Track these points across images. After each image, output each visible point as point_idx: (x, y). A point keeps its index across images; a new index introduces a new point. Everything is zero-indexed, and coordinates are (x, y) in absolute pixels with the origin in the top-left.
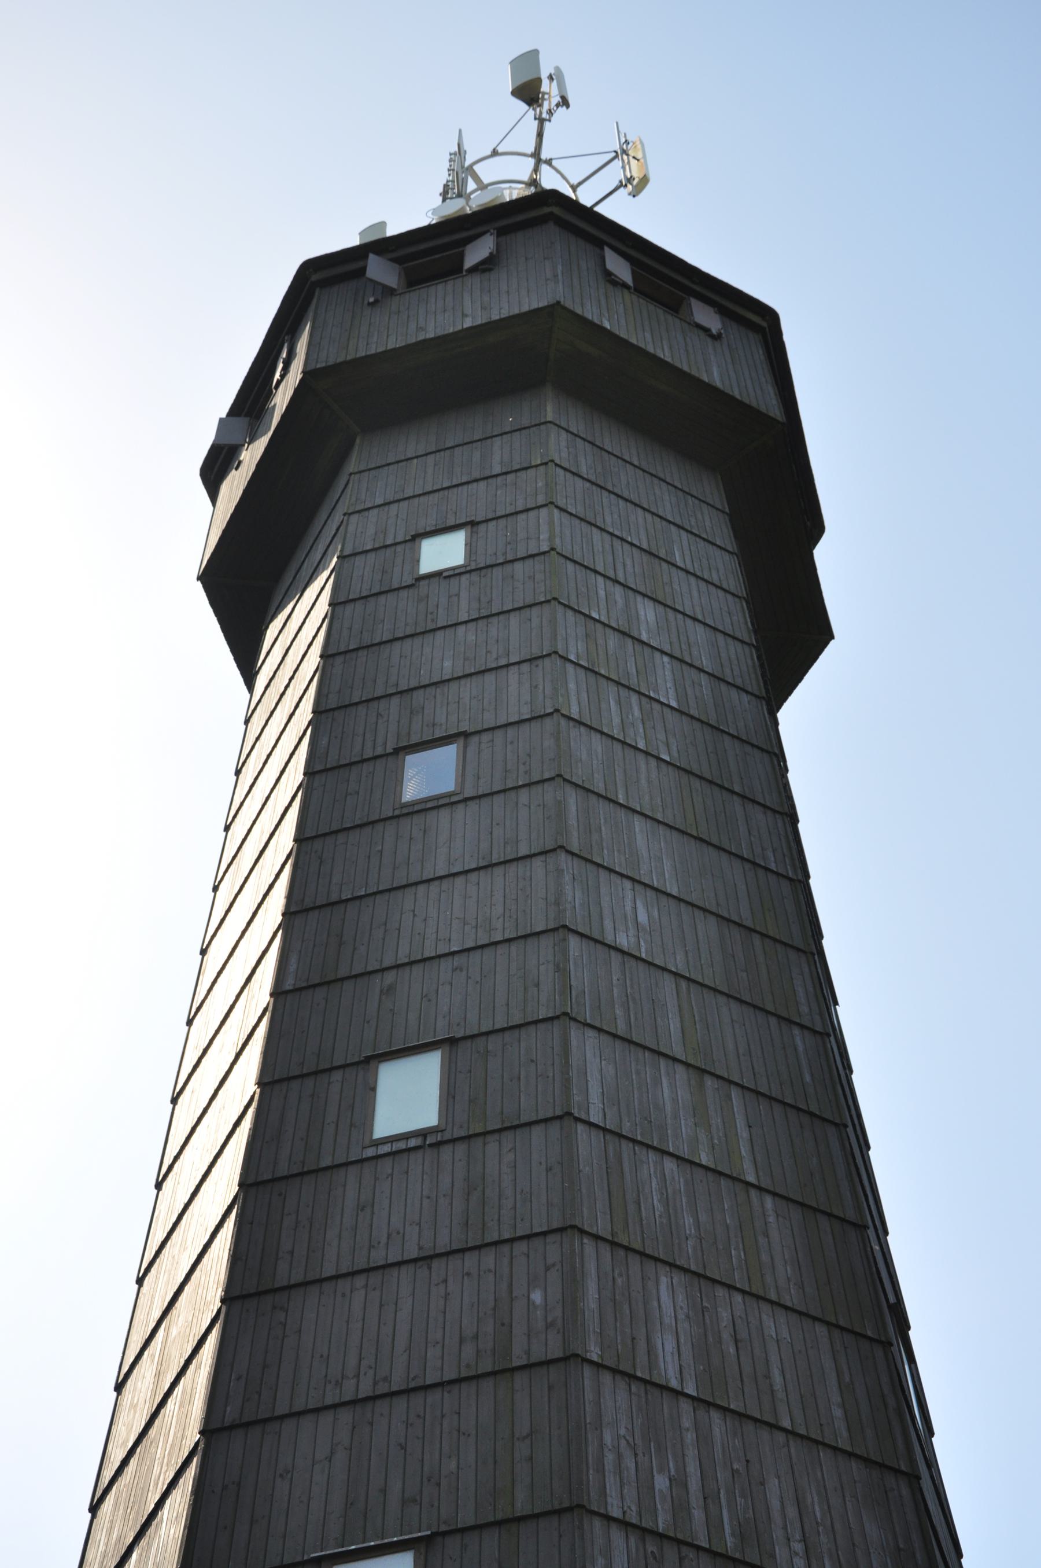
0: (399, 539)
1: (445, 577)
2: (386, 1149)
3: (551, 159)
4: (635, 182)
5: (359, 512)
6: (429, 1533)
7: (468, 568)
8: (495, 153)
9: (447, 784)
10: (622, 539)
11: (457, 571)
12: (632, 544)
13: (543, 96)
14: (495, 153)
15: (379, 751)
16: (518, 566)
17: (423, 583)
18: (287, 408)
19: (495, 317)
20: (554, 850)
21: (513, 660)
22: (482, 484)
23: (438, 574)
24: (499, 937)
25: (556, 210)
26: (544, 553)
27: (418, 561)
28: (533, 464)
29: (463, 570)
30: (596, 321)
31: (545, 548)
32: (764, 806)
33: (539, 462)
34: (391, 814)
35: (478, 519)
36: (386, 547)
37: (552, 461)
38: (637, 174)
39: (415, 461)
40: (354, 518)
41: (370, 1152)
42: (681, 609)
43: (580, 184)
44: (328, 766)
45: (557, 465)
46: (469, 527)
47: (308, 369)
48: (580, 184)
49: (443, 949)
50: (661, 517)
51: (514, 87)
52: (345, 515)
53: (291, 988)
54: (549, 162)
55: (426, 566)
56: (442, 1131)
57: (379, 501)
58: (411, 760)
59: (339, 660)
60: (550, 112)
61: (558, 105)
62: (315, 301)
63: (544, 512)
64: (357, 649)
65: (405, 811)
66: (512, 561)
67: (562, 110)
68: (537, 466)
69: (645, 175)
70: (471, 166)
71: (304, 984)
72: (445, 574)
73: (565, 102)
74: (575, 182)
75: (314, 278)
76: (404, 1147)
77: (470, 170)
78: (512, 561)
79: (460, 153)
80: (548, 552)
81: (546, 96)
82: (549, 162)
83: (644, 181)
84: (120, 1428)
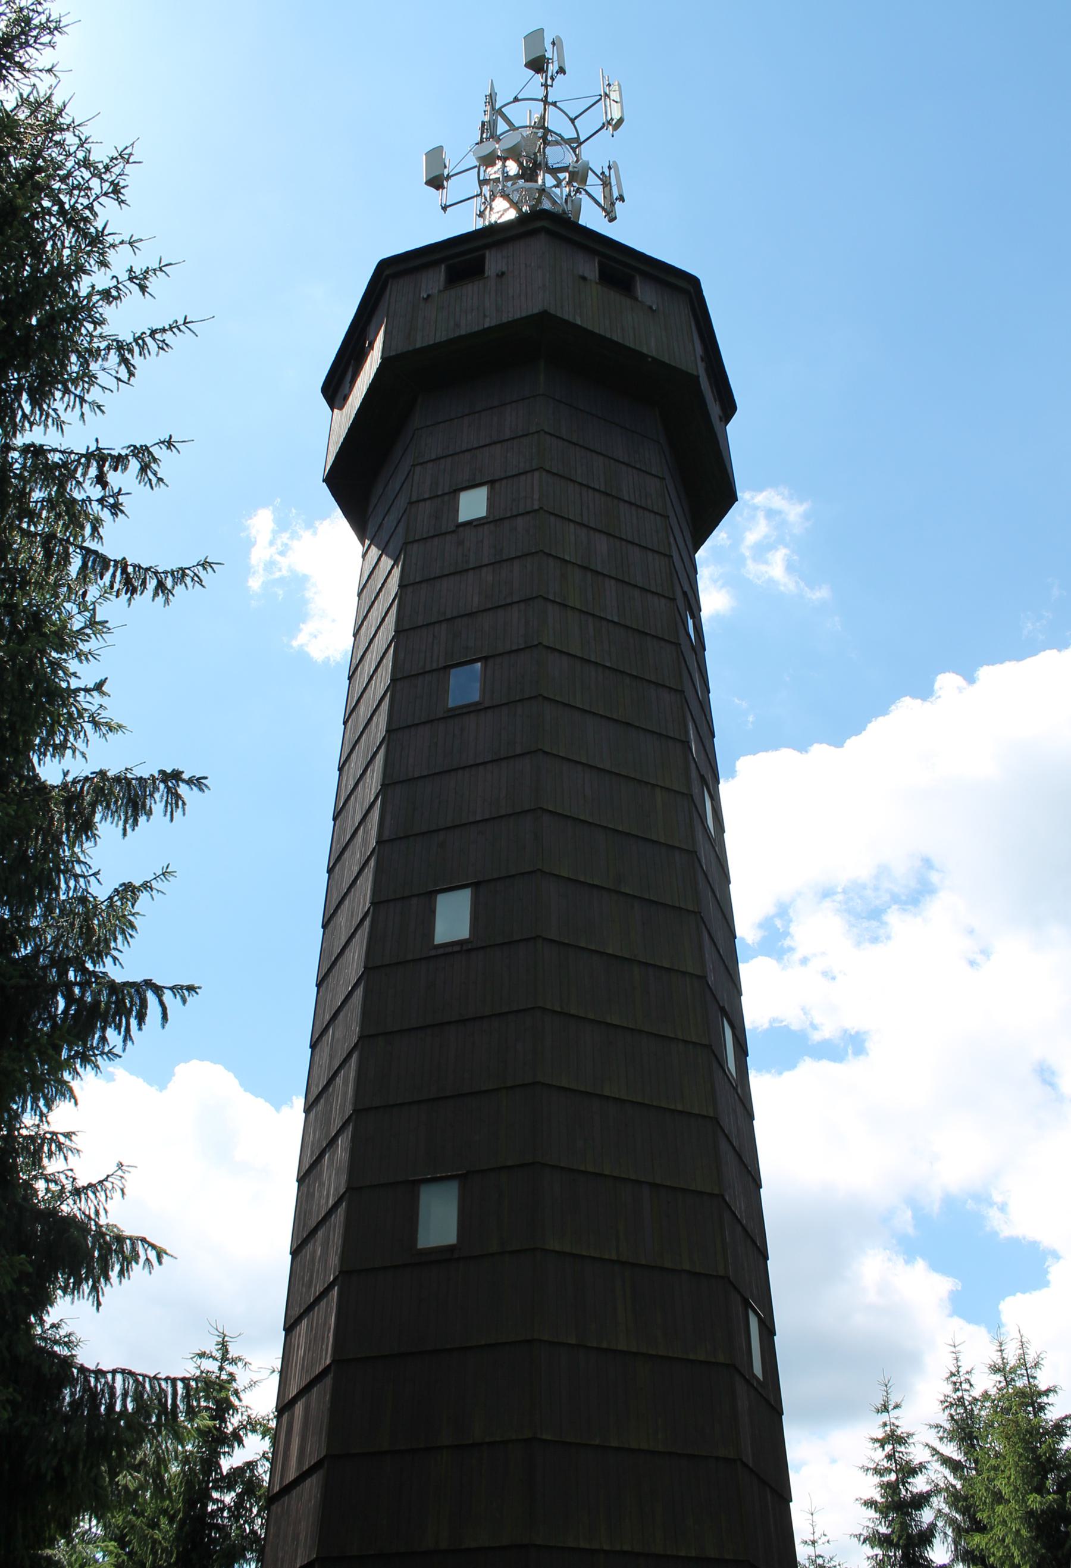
0: (446, 491)
1: (475, 526)
2: (441, 951)
3: (556, 102)
4: (614, 122)
5: (421, 464)
6: (465, 1172)
7: (489, 520)
8: (516, 100)
9: (474, 695)
10: (589, 487)
11: (482, 522)
12: (594, 489)
13: (548, 61)
14: (516, 100)
15: (435, 666)
16: (520, 520)
17: (461, 529)
18: (373, 379)
19: (505, 320)
20: (535, 751)
21: (515, 600)
22: (499, 446)
23: (469, 523)
24: (503, 813)
25: (545, 223)
26: (535, 511)
27: (458, 511)
28: (531, 432)
29: (485, 521)
30: (571, 320)
31: (536, 507)
32: (670, 688)
33: (534, 431)
34: (441, 716)
35: (497, 478)
36: (438, 496)
37: (543, 430)
38: (616, 116)
39: (456, 420)
40: (418, 469)
41: (433, 953)
42: (625, 538)
43: (576, 117)
44: (405, 675)
45: (546, 432)
46: (490, 484)
47: (385, 356)
48: (576, 117)
49: (471, 820)
50: (614, 459)
51: (528, 60)
52: (412, 466)
53: (387, 839)
54: (554, 104)
55: (464, 516)
56: (471, 942)
57: (433, 457)
58: (453, 671)
59: (410, 589)
60: (552, 79)
61: (557, 73)
62: (389, 287)
63: (537, 474)
64: (420, 582)
65: (450, 714)
66: (516, 516)
67: (560, 76)
68: (532, 433)
69: (621, 118)
70: (500, 109)
71: (394, 837)
72: (474, 524)
73: (562, 70)
74: (573, 116)
75: (387, 272)
76: (451, 951)
77: (500, 112)
78: (516, 516)
79: (491, 99)
80: (538, 510)
81: (550, 61)
82: (554, 104)
83: (621, 121)
84: (354, 661)
